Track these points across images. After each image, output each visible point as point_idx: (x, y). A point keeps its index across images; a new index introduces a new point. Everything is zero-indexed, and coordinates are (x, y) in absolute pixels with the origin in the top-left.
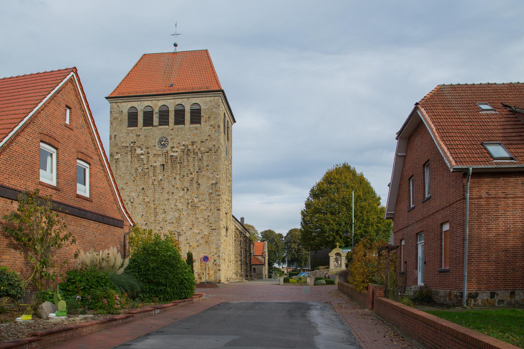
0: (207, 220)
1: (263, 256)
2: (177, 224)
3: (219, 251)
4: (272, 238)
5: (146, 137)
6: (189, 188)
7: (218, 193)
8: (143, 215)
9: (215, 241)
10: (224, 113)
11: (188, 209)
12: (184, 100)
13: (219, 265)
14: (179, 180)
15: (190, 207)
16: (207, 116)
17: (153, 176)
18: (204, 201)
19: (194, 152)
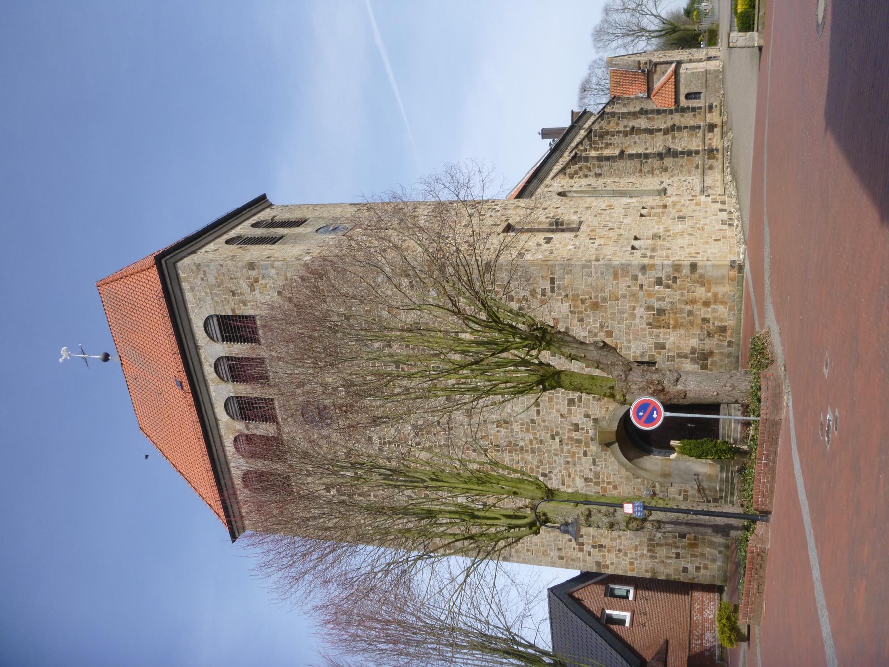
13: (677, 267)
16: (231, 298)
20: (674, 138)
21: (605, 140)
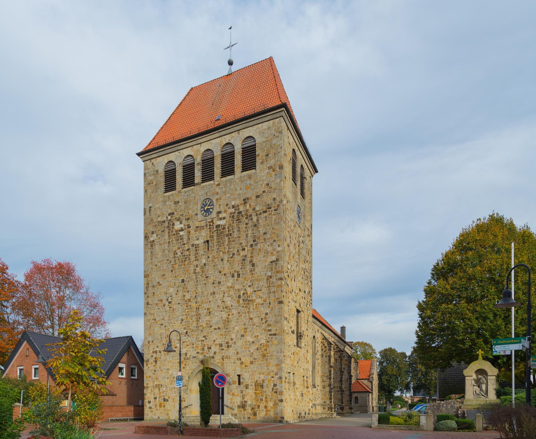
0: (264, 321)
1: (369, 379)
2: (224, 330)
3: (280, 369)
4: (393, 358)
5: (185, 202)
6: (241, 273)
7: (279, 275)
8: (182, 320)
9: (276, 353)
10: (294, 150)
11: (239, 306)
12: (233, 134)
13: (281, 393)
14: (228, 261)
15: (241, 301)
16: (264, 154)
17: (195, 260)
18: (261, 290)
19: (247, 216)
20: (338, 391)
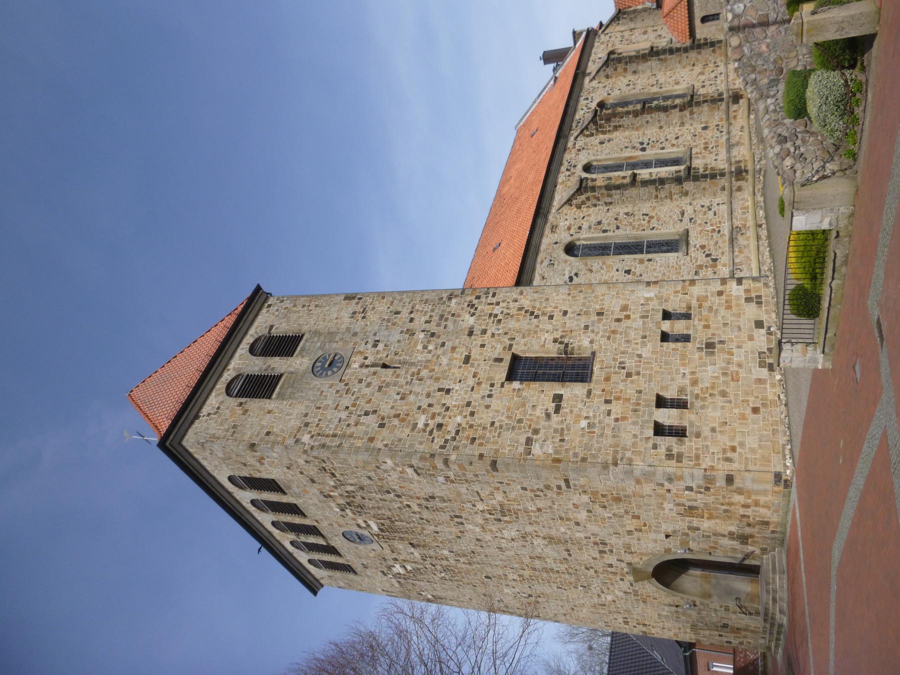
20: (692, 113)
21: (613, 122)
